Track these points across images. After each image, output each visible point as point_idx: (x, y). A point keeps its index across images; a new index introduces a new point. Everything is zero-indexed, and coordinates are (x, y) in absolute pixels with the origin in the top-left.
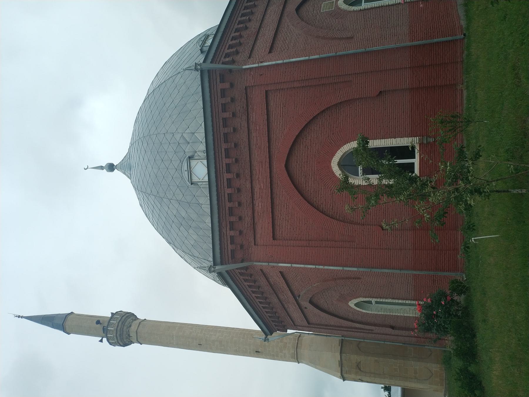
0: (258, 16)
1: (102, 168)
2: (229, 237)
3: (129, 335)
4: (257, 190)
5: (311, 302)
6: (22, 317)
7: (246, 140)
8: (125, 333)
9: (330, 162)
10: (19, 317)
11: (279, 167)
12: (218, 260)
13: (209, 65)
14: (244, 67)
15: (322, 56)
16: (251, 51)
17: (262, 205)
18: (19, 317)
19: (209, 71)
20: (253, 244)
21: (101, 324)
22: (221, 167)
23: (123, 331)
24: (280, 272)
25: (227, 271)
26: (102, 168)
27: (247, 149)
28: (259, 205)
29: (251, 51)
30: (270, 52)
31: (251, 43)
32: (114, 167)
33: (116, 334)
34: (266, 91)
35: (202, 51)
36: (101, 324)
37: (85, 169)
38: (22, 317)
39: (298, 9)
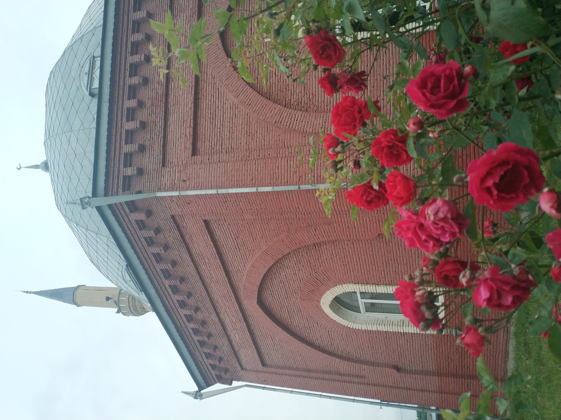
1: (37, 167)
3: (143, 308)
4: (227, 321)
6: (30, 292)
7: (194, 272)
8: (138, 307)
9: (321, 295)
10: (27, 292)
11: (251, 306)
14: (159, 194)
15: (277, 189)
16: (164, 146)
18: (27, 292)
20: (239, 368)
21: (111, 298)
22: (171, 303)
23: (135, 306)
26: (37, 167)
27: (200, 283)
28: (236, 338)
29: (164, 146)
30: (195, 152)
31: (160, 124)
33: (130, 309)
35: (92, 95)
36: (111, 298)
37: (19, 169)
38: (30, 292)
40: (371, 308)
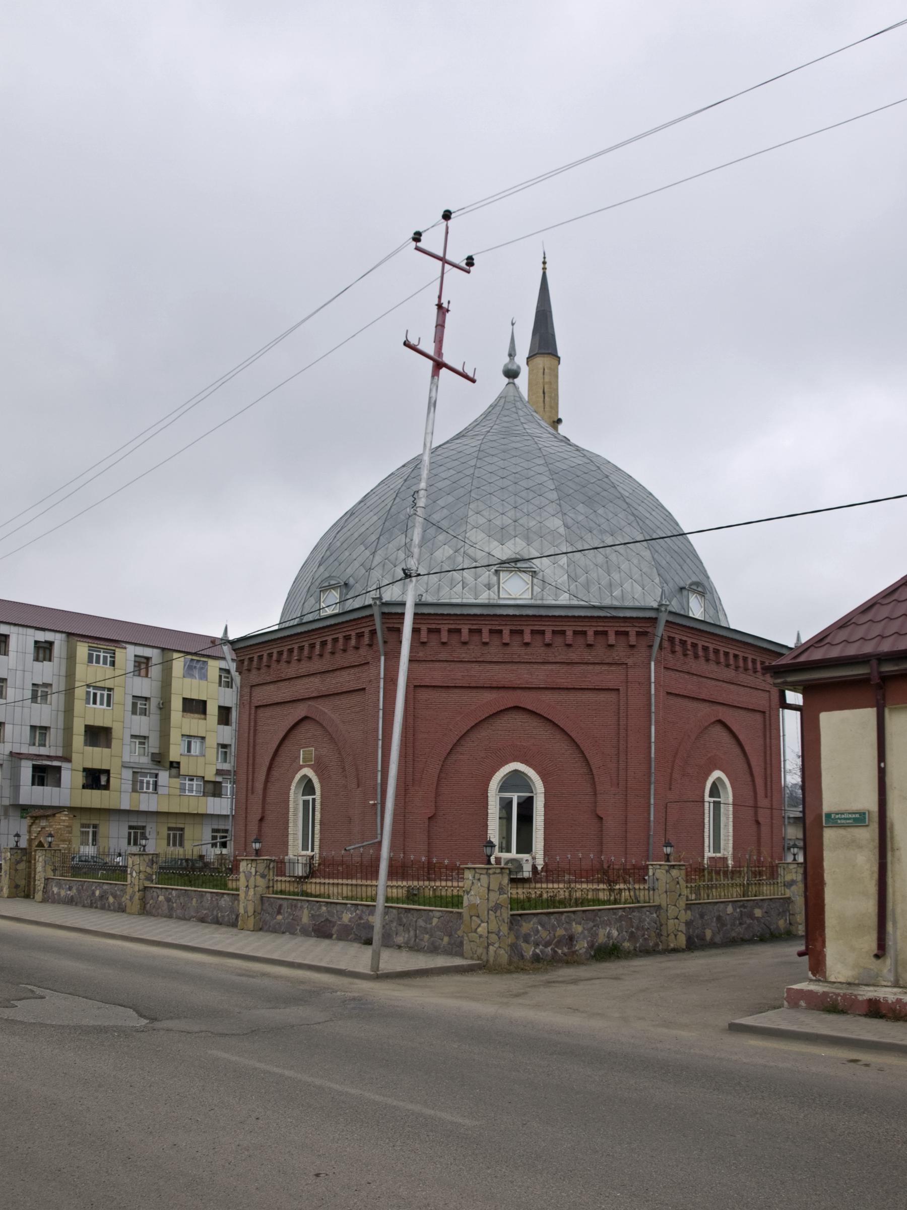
2: (606, 629)
5: (305, 718)
6: (544, 269)
11: (511, 698)
12: (386, 610)
13: (663, 618)
17: (458, 674)
19: (372, 615)
24: (364, 689)
25: (372, 615)
31: (269, 679)
32: (511, 381)
38: (544, 269)
39: (720, 722)
40: (506, 805)
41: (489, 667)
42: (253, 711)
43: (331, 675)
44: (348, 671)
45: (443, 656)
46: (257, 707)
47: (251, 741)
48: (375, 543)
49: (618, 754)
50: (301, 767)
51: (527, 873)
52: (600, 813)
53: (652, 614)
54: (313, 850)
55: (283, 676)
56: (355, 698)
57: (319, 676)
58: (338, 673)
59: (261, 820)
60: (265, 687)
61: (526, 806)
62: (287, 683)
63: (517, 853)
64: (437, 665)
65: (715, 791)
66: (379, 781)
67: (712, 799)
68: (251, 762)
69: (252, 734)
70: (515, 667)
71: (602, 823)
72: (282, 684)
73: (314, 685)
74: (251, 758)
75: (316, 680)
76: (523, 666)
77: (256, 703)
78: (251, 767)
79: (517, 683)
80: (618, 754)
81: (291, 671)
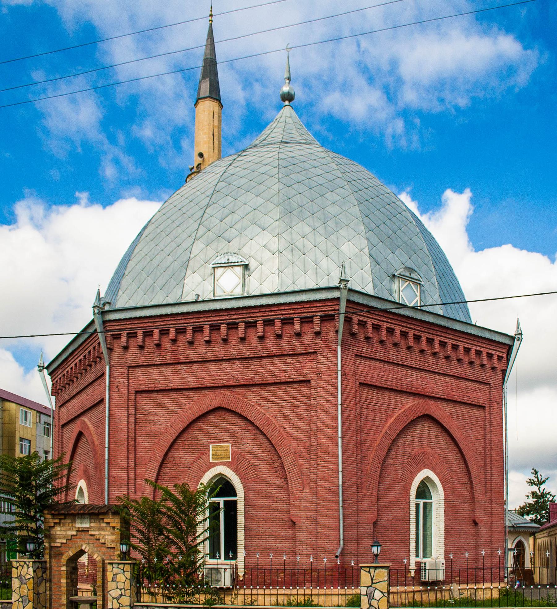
0: (442, 365)
31: (158, 360)
34: (308, 381)
41: (410, 372)
42: (132, 397)
43: (256, 362)
44: (282, 360)
45: (380, 355)
46: (137, 392)
47: (132, 432)
48: (195, 232)
49: (485, 465)
50: (212, 465)
51: (226, 581)
52: (477, 519)
53: (507, 341)
54: (417, 505)
55: (182, 358)
56: (296, 390)
57: (237, 362)
58: (267, 361)
59: (375, 523)
60: (150, 370)
61: (231, 507)
62: (187, 367)
63: (225, 560)
64: (375, 363)
65: (423, 491)
66: (340, 483)
67: (421, 502)
68: (132, 456)
69: (132, 423)
70: (426, 375)
71: (294, 529)
72: (179, 367)
73: (232, 372)
74: (132, 451)
75: (235, 367)
76: (430, 375)
77: (135, 385)
78: (132, 463)
79: (428, 391)
80: (485, 465)
81: (198, 351)
